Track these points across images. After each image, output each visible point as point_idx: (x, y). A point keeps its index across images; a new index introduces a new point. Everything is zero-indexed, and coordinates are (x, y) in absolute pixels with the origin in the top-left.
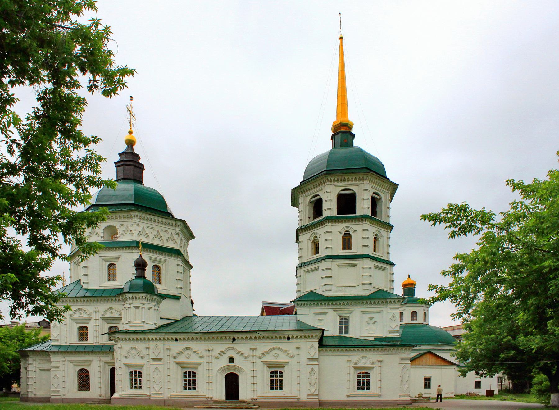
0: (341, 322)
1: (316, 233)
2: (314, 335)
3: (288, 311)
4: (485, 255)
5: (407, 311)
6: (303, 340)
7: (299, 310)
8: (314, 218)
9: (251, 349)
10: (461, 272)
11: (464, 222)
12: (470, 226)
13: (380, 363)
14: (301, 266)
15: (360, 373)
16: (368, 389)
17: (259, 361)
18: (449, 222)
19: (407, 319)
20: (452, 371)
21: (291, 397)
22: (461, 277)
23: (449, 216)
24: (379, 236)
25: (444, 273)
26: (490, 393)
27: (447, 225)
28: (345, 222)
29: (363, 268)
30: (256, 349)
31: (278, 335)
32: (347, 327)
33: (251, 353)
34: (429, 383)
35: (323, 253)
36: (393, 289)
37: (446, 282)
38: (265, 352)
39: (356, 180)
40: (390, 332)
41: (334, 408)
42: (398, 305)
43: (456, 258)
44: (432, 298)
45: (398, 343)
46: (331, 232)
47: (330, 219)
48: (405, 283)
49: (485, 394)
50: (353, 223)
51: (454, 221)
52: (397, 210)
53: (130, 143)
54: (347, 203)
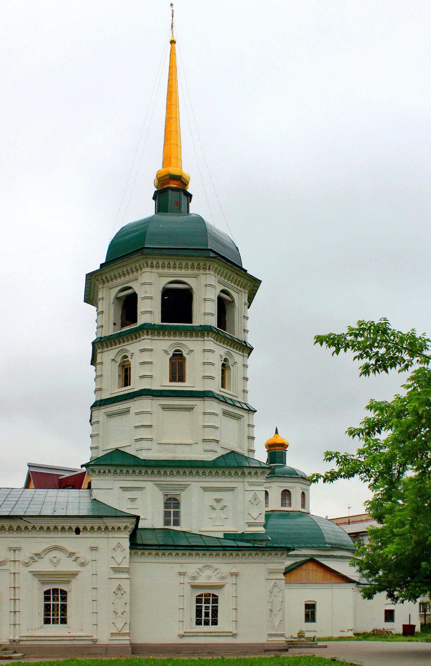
0: (167, 505)
1: (126, 351)
2: (122, 525)
3: (74, 482)
4: (417, 405)
5: (276, 489)
6: (103, 535)
7: (97, 481)
8: (123, 326)
9: (10, 549)
10: (379, 432)
11: (382, 351)
12: (392, 358)
13: (234, 577)
14: (99, 404)
15: (201, 595)
16: (215, 623)
17: (24, 571)
18: (359, 349)
19: (275, 503)
20: (349, 595)
21: (81, 638)
22: (376, 440)
23: (360, 339)
24: (230, 363)
25: (352, 433)
26: (409, 630)
27: (357, 353)
28: (175, 335)
29: (205, 413)
30: (19, 549)
31: (60, 524)
32: (177, 514)
33: (11, 556)
34: (313, 614)
35: (136, 385)
36: (253, 451)
37: (353, 447)
38: (37, 555)
39: (193, 267)
40: (250, 525)
41: (158, 658)
42: (261, 479)
43: (370, 407)
44: (330, 472)
45: (264, 544)
46: (151, 350)
47: (148, 329)
48: (270, 442)
49: (401, 631)
50: (188, 338)
51: (367, 347)
52: (256, 320)
54: (177, 305)
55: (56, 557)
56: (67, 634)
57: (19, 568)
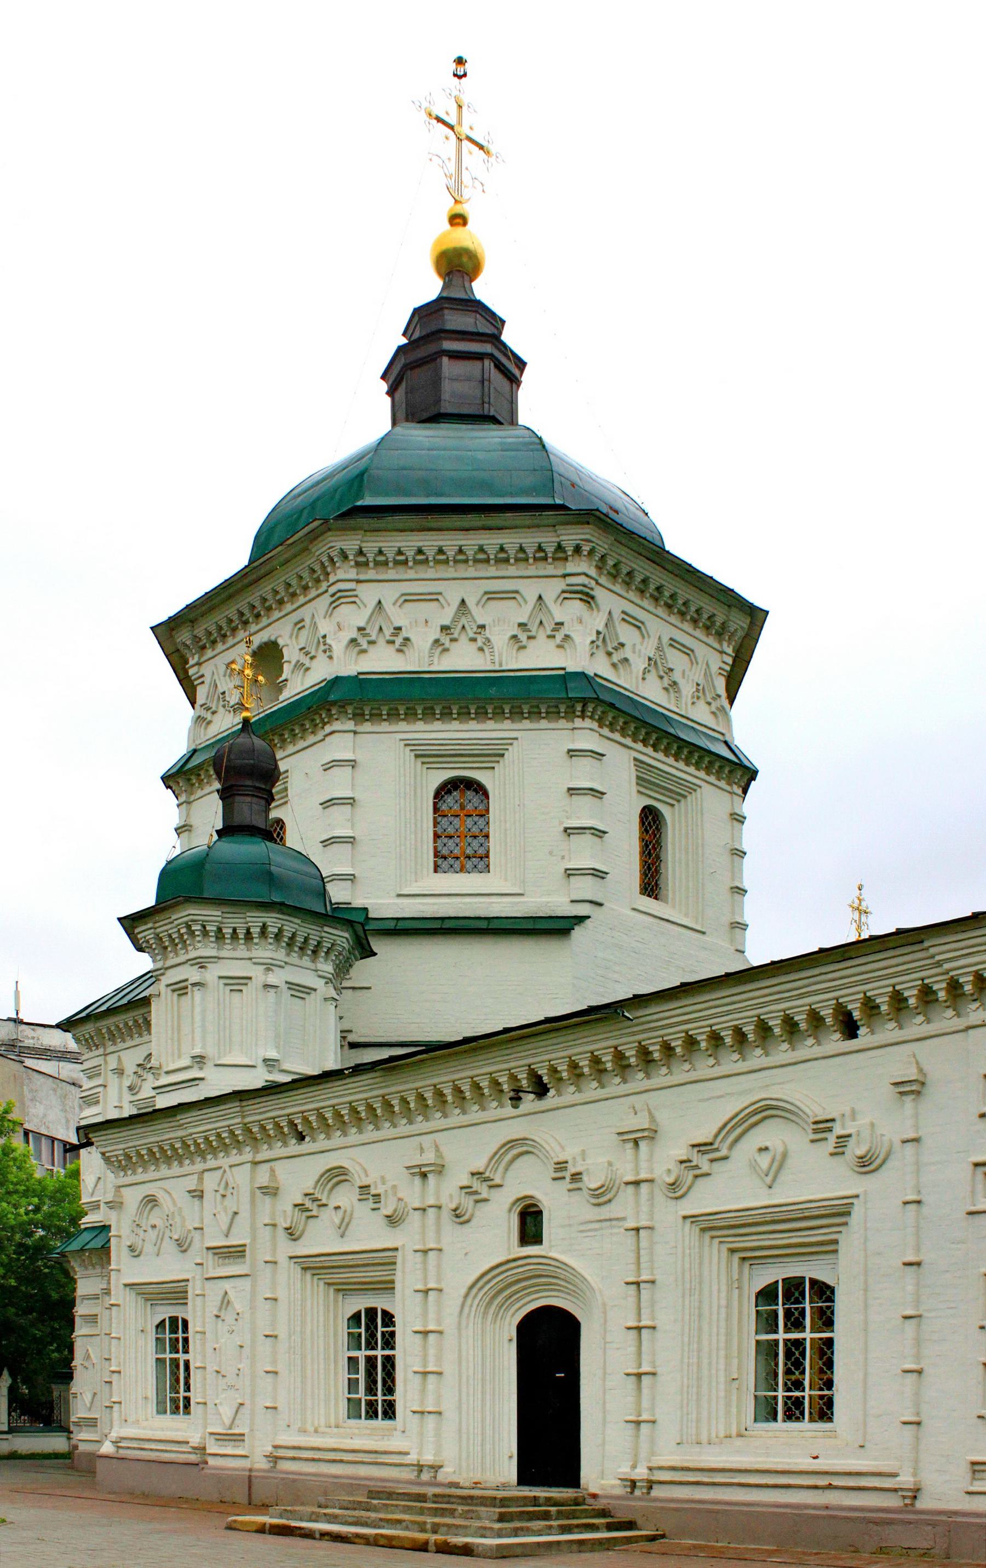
17: (668, 1215)
34: (539, 1225)
53: (457, 266)
55: (766, 1149)
56: (807, 1463)
57: (652, 1205)
